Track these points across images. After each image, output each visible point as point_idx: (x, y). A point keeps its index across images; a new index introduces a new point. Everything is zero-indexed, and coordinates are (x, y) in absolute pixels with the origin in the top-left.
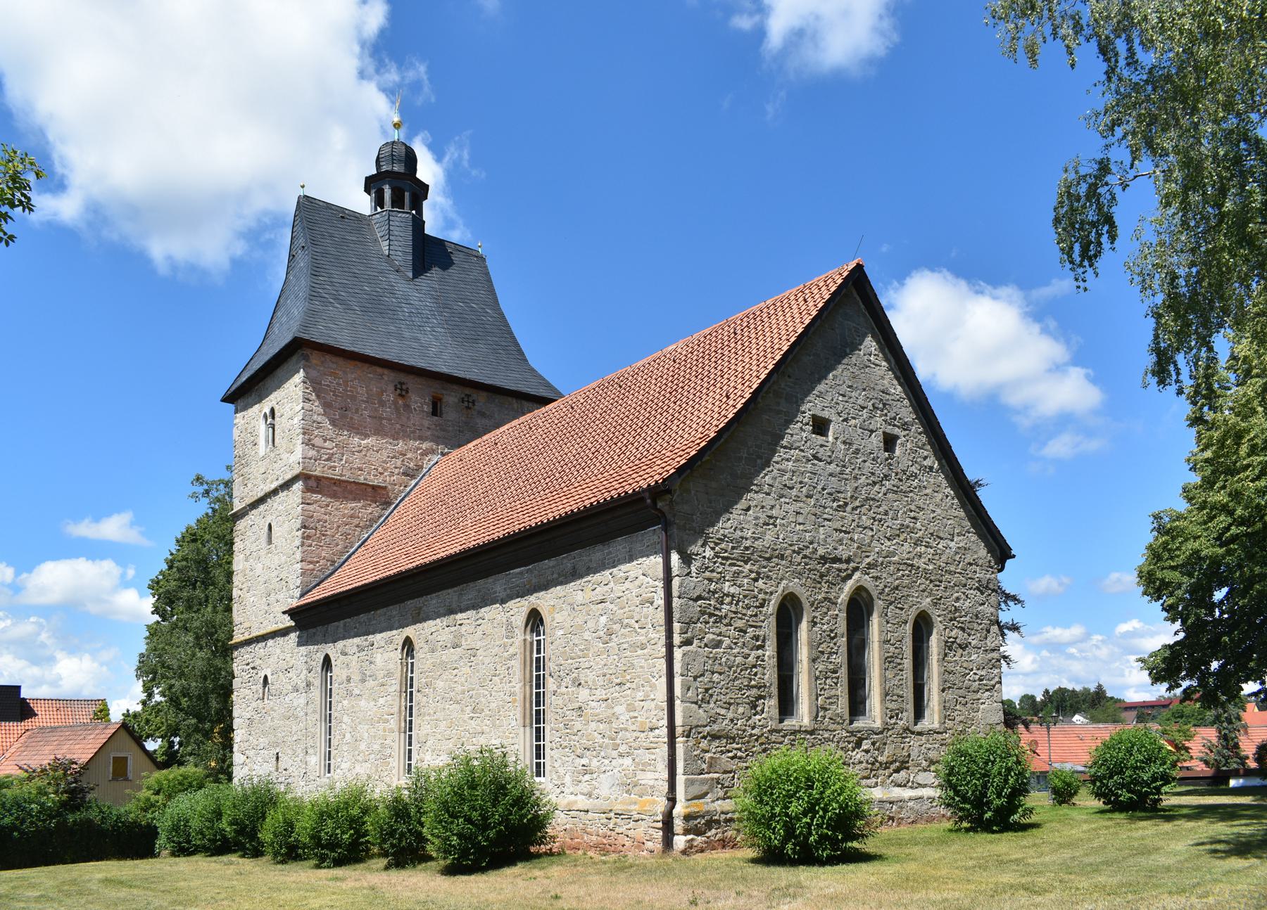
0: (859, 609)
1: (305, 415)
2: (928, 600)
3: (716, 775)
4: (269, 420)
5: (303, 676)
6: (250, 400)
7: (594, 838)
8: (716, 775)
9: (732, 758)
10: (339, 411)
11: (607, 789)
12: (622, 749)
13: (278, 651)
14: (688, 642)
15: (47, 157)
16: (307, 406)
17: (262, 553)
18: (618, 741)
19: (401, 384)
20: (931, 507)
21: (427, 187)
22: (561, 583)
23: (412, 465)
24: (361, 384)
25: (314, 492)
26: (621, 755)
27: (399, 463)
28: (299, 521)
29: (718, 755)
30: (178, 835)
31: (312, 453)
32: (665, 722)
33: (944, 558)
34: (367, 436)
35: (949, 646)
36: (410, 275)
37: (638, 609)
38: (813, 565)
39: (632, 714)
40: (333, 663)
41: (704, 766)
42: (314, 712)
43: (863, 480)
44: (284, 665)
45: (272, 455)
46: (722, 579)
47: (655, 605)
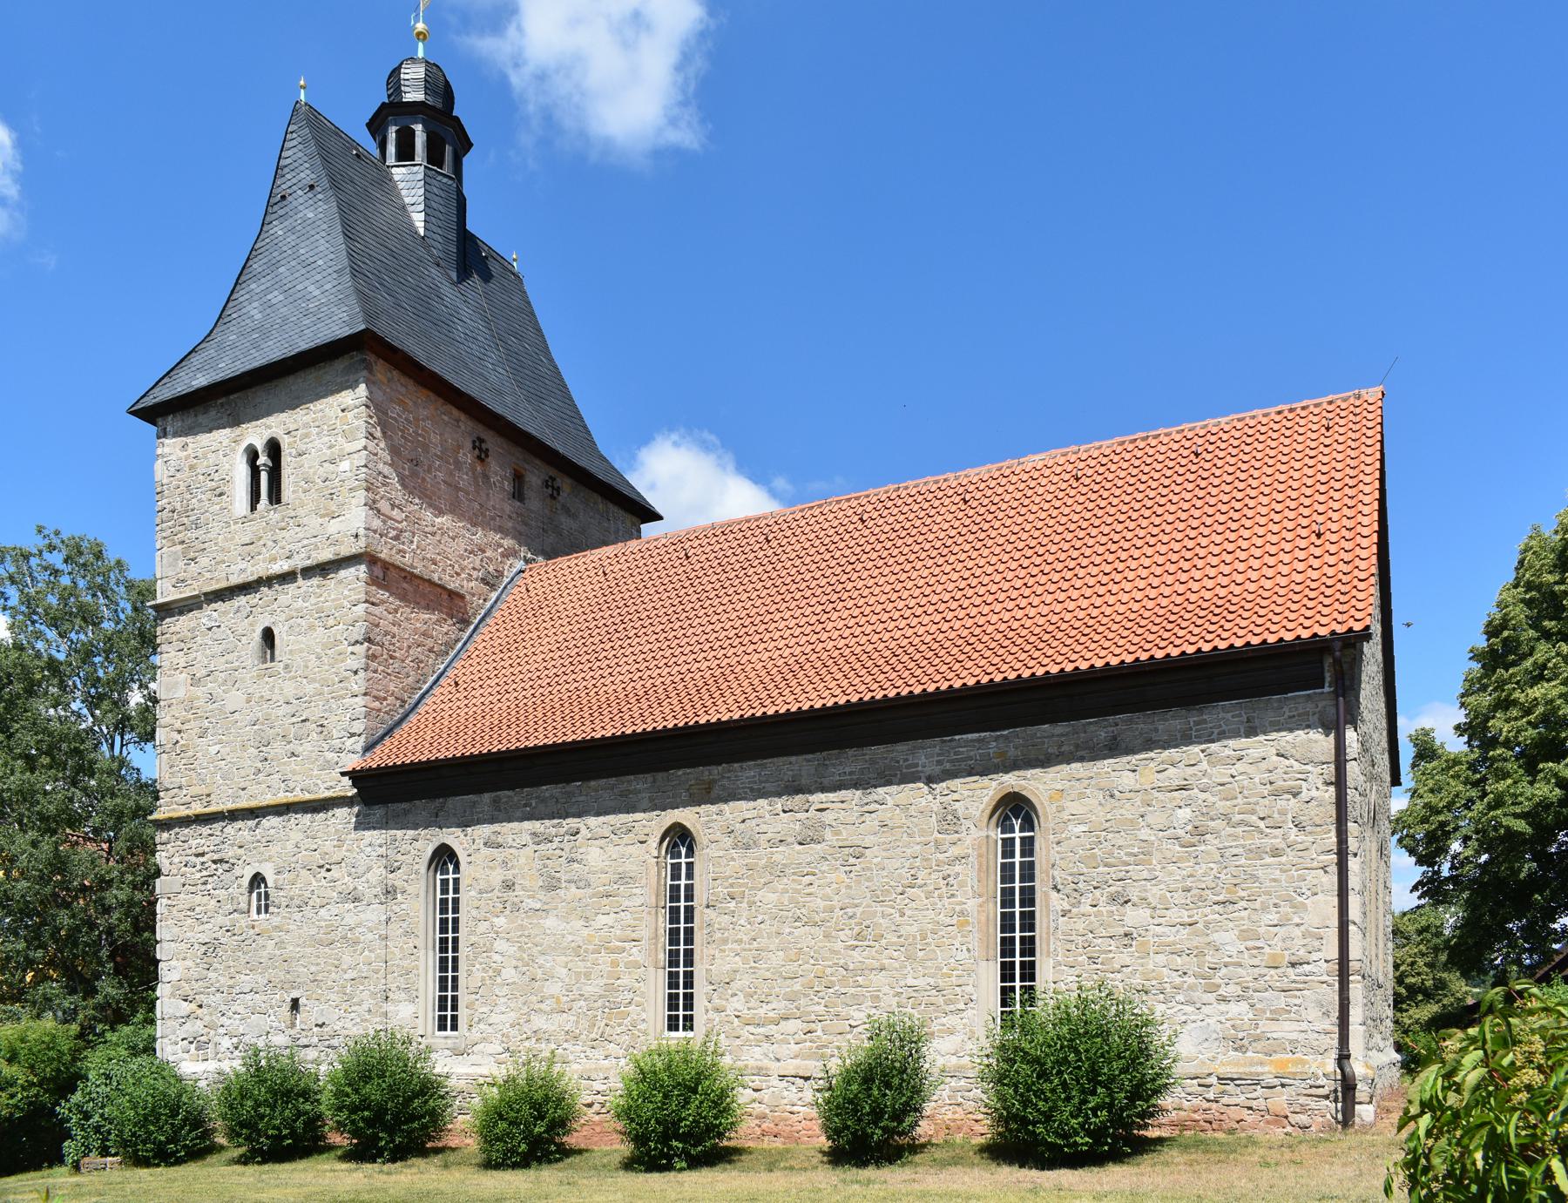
6: (201, 419)
10: (411, 467)
16: (371, 445)
18: (1217, 980)
19: (482, 441)
22: (1081, 759)
24: (444, 432)
25: (380, 586)
30: (239, 1135)
31: (377, 523)
34: (440, 513)
36: (454, 275)
39: (1250, 944)
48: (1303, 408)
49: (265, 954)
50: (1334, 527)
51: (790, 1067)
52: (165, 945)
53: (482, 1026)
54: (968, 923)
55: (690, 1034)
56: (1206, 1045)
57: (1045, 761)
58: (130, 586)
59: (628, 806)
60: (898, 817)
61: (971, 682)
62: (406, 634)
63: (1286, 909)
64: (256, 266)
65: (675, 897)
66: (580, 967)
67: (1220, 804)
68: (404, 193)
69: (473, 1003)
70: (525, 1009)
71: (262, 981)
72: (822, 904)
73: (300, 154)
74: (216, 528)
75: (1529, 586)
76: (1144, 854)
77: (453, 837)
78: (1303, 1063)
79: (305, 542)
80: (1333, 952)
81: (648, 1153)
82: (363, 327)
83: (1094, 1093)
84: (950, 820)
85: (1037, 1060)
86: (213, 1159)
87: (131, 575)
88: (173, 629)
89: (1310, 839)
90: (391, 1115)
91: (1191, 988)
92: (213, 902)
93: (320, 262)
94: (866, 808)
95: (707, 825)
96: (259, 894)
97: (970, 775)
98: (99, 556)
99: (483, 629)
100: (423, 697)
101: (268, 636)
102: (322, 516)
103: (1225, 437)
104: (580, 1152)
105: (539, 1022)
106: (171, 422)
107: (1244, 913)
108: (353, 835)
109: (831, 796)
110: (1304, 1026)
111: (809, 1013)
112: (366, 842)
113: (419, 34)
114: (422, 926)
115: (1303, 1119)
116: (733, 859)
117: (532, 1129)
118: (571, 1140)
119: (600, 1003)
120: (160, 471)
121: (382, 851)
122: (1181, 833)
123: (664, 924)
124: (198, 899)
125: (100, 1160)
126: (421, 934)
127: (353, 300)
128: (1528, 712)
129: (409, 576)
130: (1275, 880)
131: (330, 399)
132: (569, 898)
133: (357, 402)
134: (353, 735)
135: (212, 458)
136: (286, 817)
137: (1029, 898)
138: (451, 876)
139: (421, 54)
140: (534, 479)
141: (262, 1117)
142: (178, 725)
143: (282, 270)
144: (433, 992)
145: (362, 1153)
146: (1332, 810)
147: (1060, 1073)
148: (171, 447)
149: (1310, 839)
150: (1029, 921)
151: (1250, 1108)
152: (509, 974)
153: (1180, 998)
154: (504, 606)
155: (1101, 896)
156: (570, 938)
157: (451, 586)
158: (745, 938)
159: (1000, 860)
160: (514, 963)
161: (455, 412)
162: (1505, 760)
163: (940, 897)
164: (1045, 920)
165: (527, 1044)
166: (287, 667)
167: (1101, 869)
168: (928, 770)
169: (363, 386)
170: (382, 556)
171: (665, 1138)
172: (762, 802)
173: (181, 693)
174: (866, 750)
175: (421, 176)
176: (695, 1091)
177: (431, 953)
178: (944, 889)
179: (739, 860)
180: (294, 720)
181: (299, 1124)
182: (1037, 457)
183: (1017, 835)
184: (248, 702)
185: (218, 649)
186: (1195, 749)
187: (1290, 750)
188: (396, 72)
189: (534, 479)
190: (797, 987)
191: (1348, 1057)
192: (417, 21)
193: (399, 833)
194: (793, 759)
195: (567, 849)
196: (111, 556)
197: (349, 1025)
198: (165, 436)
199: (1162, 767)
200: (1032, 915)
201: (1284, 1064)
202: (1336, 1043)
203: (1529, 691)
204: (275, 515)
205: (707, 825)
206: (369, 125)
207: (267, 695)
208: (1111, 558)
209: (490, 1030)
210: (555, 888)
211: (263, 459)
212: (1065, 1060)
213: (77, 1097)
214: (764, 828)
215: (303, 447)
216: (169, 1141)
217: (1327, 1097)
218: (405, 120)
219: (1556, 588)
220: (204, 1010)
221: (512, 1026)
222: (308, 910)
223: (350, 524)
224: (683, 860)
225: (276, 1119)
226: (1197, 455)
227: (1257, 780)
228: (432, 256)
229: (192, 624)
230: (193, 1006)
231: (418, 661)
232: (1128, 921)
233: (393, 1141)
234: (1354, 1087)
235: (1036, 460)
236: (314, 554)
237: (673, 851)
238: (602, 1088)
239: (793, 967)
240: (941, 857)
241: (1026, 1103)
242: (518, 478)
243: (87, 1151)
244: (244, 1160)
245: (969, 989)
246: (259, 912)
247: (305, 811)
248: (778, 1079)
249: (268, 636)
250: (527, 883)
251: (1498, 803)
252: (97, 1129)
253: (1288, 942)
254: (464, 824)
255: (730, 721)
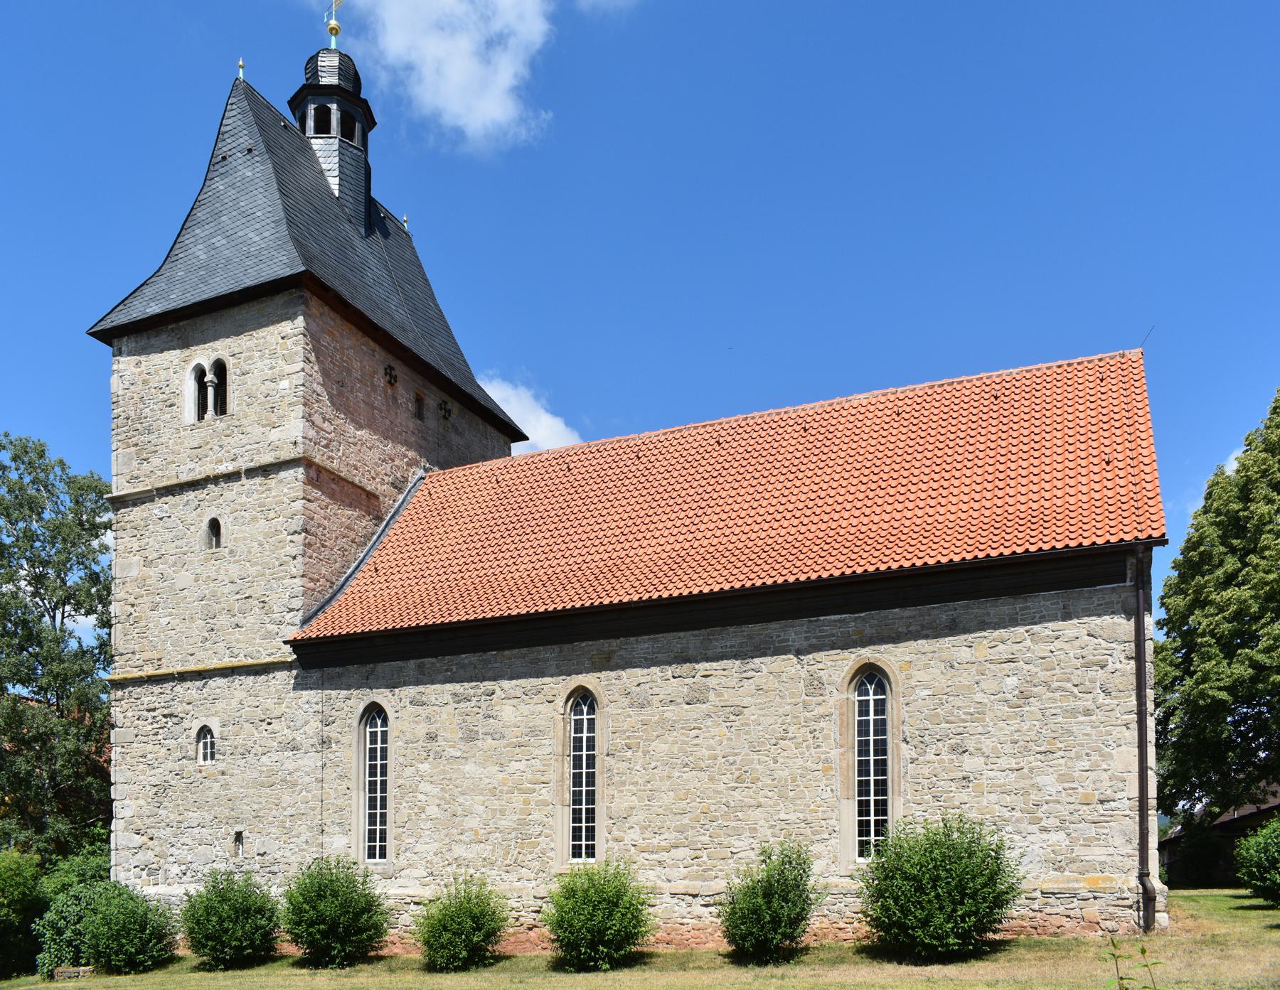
10: (338, 386)
16: (307, 367)
18: (1040, 815)
19: (392, 368)
21: (375, 124)
22: (926, 637)
24: (363, 360)
25: (315, 486)
30: (205, 946)
31: (312, 433)
34: (360, 427)
36: (362, 231)
39: (1067, 785)
48: (1079, 364)
49: (211, 794)
50: (1120, 457)
51: (680, 886)
52: (119, 786)
53: (408, 854)
54: (831, 768)
55: (591, 860)
57: (896, 638)
58: (71, 482)
59: (538, 672)
60: (772, 683)
61: (737, 585)
62: (334, 527)
63: (1095, 757)
64: (200, 214)
65: (578, 747)
66: (496, 804)
67: (1041, 674)
68: (321, 160)
69: (400, 835)
70: (447, 840)
71: (209, 817)
72: (707, 753)
73: (239, 123)
74: (166, 434)
75: (1218, 512)
76: (979, 714)
77: (383, 697)
78: (1111, 880)
79: (249, 447)
80: (1135, 793)
81: (578, 957)
82: (303, 268)
83: (962, 903)
84: (816, 686)
85: (914, 878)
86: (175, 967)
87: (72, 473)
88: (126, 518)
89: (1115, 702)
90: (339, 927)
91: (1018, 820)
92: (164, 750)
93: (259, 214)
94: (745, 675)
95: (607, 688)
96: (205, 744)
97: (833, 648)
98: (41, 455)
99: (393, 525)
100: (347, 579)
101: (215, 526)
102: (264, 426)
103: (1018, 384)
104: (508, 958)
105: (459, 851)
106: (126, 343)
107: (1062, 761)
108: (292, 694)
109: (714, 665)
110: (1111, 850)
111: (696, 842)
112: (304, 699)
113: (332, 29)
114: (354, 771)
115: (1109, 924)
116: (630, 716)
117: (466, 937)
118: (500, 948)
119: (513, 835)
120: (116, 384)
121: (319, 707)
122: (1009, 696)
123: (569, 770)
124: (150, 747)
125: (72, 969)
126: (354, 777)
127: (290, 246)
128: (1221, 610)
129: (336, 478)
130: (1087, 735)
131: (271, 328)
132: (486, 748)
133: (296, 331)
134: (291, 610)
135: (163, 375)
136: (231, 679)
137: (881, 748)
138: (379, 729)
139: (333, 46)
140: (431, 402)
141: (226, 931)
142: (131, 600)
143: (223, 218)
144: (364, 826)
145: (316, 959)
146: (1133, 679)
147: (934, 887)
148: (126, 365)
149: (1115, 702)
150: (882, 767)
151: (1068, 916)
152: (432, 810)
153: (1009, 829)
154: (410, 506)
155: (944, 747)
156: (487, 781)
157: (369, 488)
158: (641, 781)
159: (857, 718)
160: (437, 801)
161: (372, 344)
162: (1210, 646)
163: (808, 748)
164: (896, 767)
165: (448, 869)
166: (231, 552)
167: (943, 725)
168: (797, 645)
169: (301, 318)
170: (316, 460)
171: (593, 945)
172: (654, 669)
173: (134, 573)
174: (744, 628)
175: (336, 147)
176: (616, 905)
177: (362, 793)
178: (811, 741)
179: (635, 717)
180: (238, 596)
181: (258, 936)
182: (862, 396)
183: (871, 697)
184: (196, 581)
185: (168, 536)
186: (1021, 629)
187: (1098, 631)
188: (313, 59)
189: (431, 402)
190: (686, 821)
191: (1148, 875)
192: (330, 18)
193: (334, 693)
194: (682, 634)
195: (484, 707)
196: (52, 456)
197: (288, 854)
198: (120, 354)
199: (993, 644)
200: (884, 762)
201: (1096, 880)
202: (1137, 864)
203: (1224, 593)
204: (221, 424)
205: (607, 688)
206: (291, 103)
207: (213, 575)
208: (823, 494)
209: (415, 857)
210: (473, 739)
211: (210, 377)
212: (938, 878)
213: (49, 916)
214: (656, 690)
215: (247, 368)
216: (138, 953)
217: (1130, 907)
218: (322, 100)
219: (1241, 514)
220: (155, 842)
221: (435, 854)
222: (250, 757)
223: (290, 433)
224: (585, 717)
225: (235, 931)
226: (996, 398)
227: (1071, 655)
228: (345, 214)
229: (145, 514)
230: (145, 839)
231: (342, 549)
232: (966, 767)
233: (344, 950)
234: (1154, 899)
235: (861, 398)
236: (256, 458)
237: (576, 709)
238: (515, 905)
239: (683, 805)
240: (809, 715)
241: (905, 912)
242: (419, 401)
243: (60, 962)
244: (202, 967)
245: (833, 822)
246: (205, 759)
247: (249, 674)
248: (683, 898)
249: (215, 526)
250: (448, 735)
251: (1205, 679)
252: (69, 943)
253: (1098, 784)
254: (392, 686)
255: (630, 602)
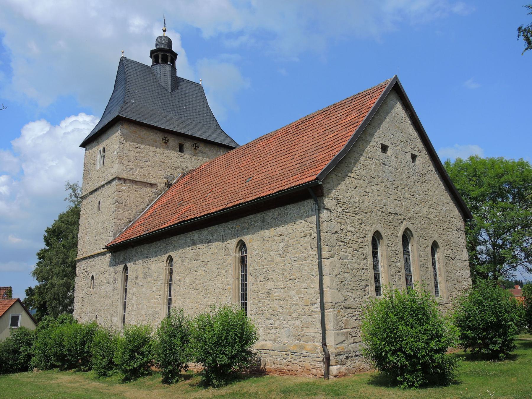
0: (406, 237)
1: (120, 150)
2: (436, 235)
3: (349, 330)
4: (102, 153)
5: (112, 276)
7: (279, 366)
8: (349, 330)
9: (356, 320)
11: (286, 340)
12: (295, 315)
13: (100, 263)
14: (332, 257)
15: (26, 330)
16: (121, 146)
17: (95, 215)
18: (291, 311)
20: (434, 190)
23: (169, 174)
26: (294, 319)
27: (163, 173)
28: (114, 200)
29: (349, 319)
31: (122, 168)
32: (319, 300)
33: (441, 214)
35: (447, 257)
37: (302, 239)
38: (386, 217)
39: (300, 296)
40: (129, 269)
41: (343, 325)
42: (118, 294)
43: (404, 176)
44: (102, 270)
45: (102, 169)
46: (345, 223)
47: (312, 237)
56: (289, 337)
84: (227, 251)
107: (298, 283)
130: (305, 270)
